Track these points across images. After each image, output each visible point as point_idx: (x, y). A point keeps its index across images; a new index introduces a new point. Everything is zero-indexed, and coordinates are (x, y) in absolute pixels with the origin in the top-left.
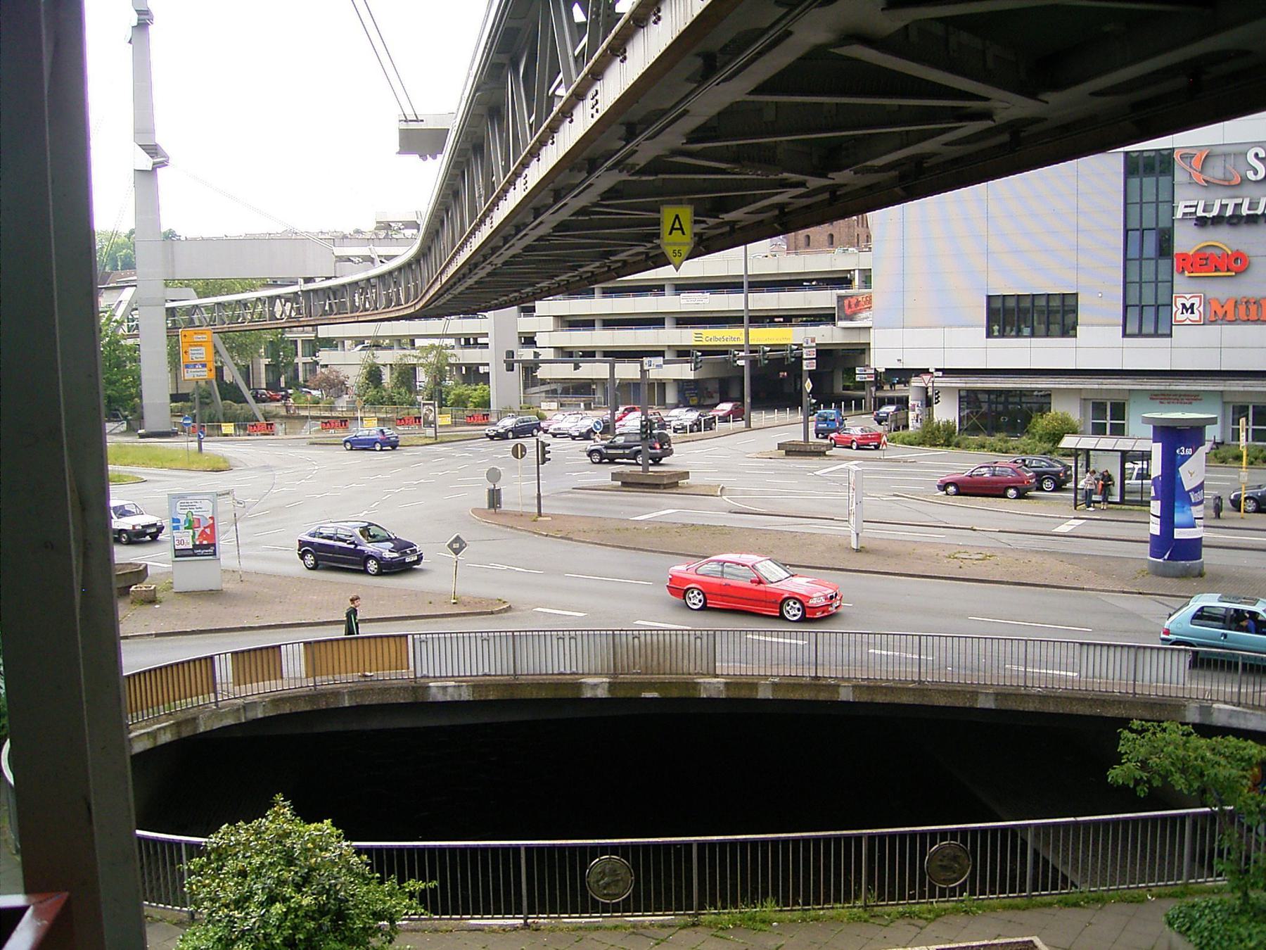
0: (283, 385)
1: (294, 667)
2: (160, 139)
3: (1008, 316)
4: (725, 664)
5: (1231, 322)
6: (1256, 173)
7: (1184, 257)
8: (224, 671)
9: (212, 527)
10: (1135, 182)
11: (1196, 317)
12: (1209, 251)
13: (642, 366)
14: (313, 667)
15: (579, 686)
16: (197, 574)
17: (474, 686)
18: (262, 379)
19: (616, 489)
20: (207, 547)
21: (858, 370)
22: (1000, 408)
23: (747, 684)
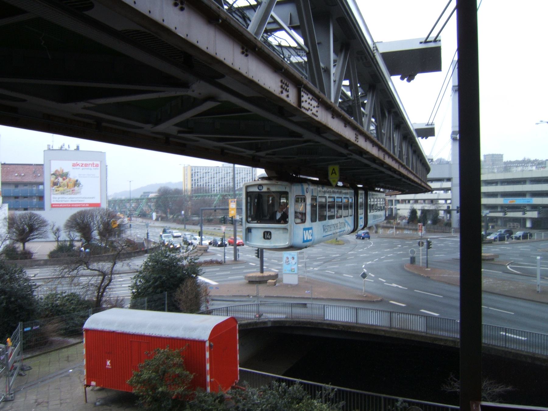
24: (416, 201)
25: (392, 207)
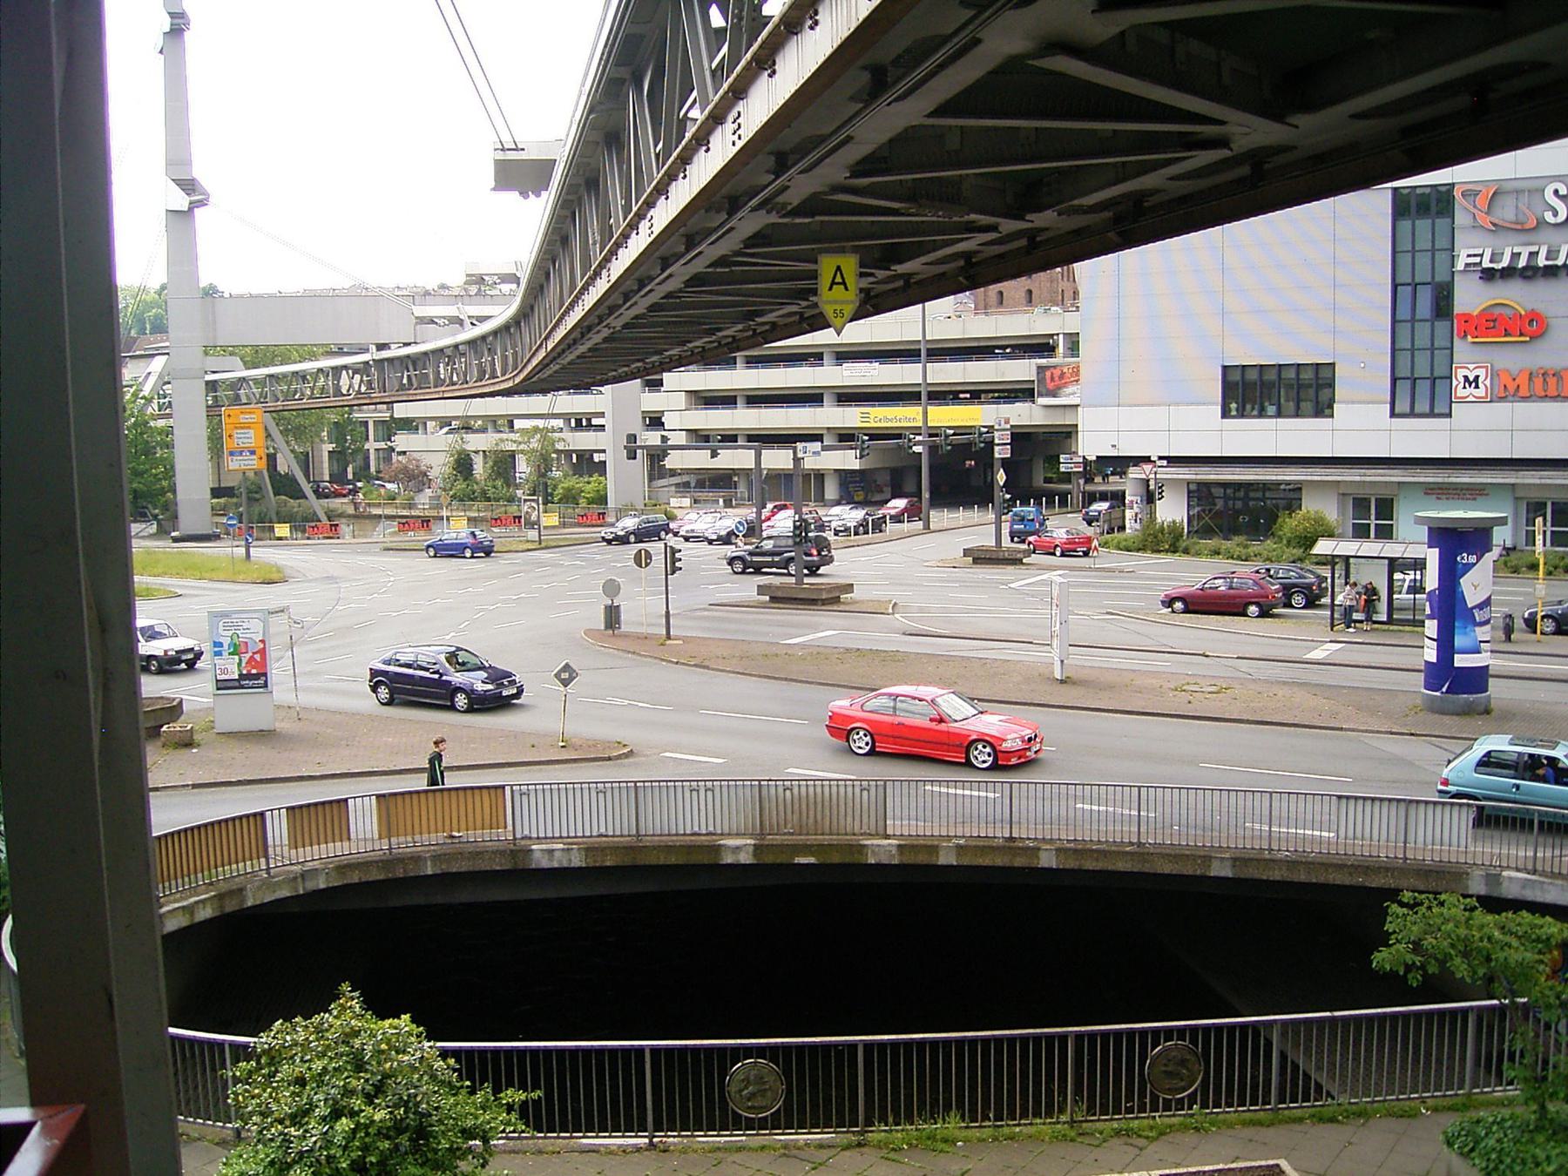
0: (350, 477)
1: (364, 826)
2: (199, 172)
3: (1248, 391)
4: (898, 822)
5: (1525, 399)
6: (1556, 214)
7: (1467, 318)
8: (278, 830)
9: (263, 652)
10: (1406, 225)
11: (1481, 392)
12: (1497, 311)
13: (795, 453)
14: (388, 826)
15: (717, 849)
16: (244, 710)
17: (587, 850)
18: (325, 470)
19: (763, 605)
20: (257, 677)
21: (1062, 458)
22: (1239, 505)
23: (926, 846)
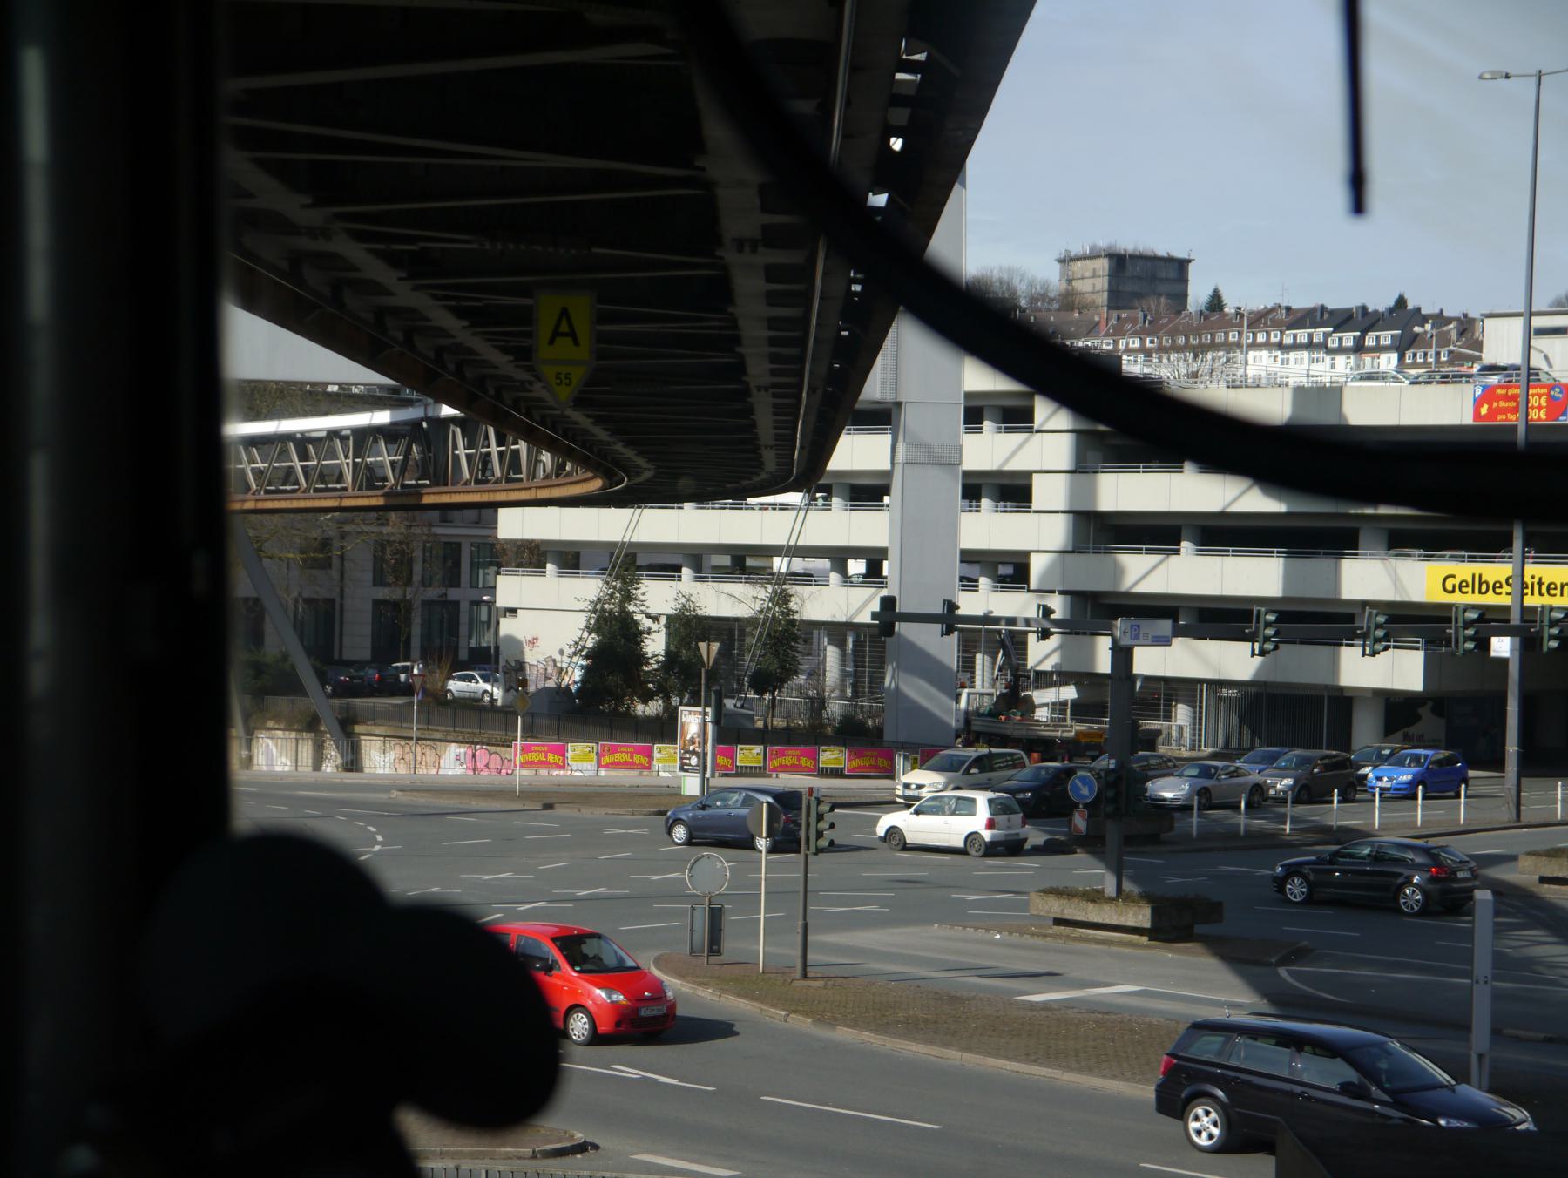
10: (1103, 265)
24: (629, 564)
25: (454, 594)
